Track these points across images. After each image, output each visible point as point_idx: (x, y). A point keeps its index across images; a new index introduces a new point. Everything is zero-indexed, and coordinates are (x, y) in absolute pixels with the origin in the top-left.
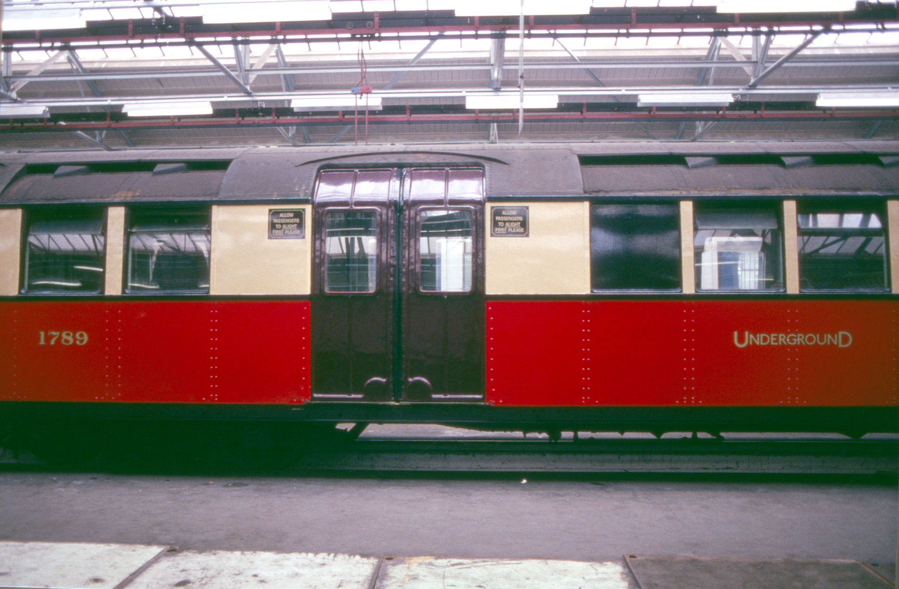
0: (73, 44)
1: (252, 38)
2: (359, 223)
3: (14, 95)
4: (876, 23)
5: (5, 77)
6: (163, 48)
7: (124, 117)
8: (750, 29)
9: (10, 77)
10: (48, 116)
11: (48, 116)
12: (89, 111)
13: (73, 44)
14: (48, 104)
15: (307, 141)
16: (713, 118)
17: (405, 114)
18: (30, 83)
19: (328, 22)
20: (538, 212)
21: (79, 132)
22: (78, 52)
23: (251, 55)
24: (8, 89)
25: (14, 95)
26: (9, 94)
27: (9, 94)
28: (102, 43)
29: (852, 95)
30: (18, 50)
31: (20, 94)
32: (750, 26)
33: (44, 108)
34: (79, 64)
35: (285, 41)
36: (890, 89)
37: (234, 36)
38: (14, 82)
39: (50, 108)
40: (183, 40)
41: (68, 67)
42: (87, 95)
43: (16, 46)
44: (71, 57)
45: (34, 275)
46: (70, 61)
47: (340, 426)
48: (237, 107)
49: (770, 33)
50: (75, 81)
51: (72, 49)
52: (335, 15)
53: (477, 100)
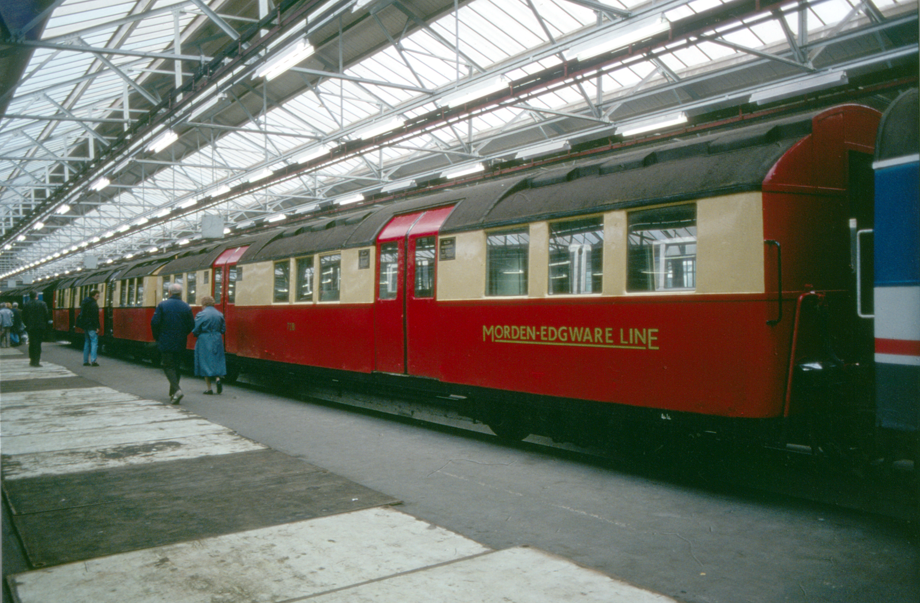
0: (654, 51)
3: (810, 66)
4: (642, 53)
5: (801, 48)
6: (752, 28)
11: (416, 185)
13: (654, 51)
14: (570, 138)
17: (738, 114)
18: (829, 47)
20: (702, 205)
25: (810, 66)
26: (805, 65)
27: (805, 65)
28: (746, 21)
29: (663, 118)
30: (607, 72)
31: (480, 152)
33: (841, 73)
35: (584, 79)
36: (830, 70)
37: (574, 77)
40: (769, 13)
42: (888, 48)
43: (604, 68)
45: (566, 280)
47: (817, 366)
50: (671, 90)
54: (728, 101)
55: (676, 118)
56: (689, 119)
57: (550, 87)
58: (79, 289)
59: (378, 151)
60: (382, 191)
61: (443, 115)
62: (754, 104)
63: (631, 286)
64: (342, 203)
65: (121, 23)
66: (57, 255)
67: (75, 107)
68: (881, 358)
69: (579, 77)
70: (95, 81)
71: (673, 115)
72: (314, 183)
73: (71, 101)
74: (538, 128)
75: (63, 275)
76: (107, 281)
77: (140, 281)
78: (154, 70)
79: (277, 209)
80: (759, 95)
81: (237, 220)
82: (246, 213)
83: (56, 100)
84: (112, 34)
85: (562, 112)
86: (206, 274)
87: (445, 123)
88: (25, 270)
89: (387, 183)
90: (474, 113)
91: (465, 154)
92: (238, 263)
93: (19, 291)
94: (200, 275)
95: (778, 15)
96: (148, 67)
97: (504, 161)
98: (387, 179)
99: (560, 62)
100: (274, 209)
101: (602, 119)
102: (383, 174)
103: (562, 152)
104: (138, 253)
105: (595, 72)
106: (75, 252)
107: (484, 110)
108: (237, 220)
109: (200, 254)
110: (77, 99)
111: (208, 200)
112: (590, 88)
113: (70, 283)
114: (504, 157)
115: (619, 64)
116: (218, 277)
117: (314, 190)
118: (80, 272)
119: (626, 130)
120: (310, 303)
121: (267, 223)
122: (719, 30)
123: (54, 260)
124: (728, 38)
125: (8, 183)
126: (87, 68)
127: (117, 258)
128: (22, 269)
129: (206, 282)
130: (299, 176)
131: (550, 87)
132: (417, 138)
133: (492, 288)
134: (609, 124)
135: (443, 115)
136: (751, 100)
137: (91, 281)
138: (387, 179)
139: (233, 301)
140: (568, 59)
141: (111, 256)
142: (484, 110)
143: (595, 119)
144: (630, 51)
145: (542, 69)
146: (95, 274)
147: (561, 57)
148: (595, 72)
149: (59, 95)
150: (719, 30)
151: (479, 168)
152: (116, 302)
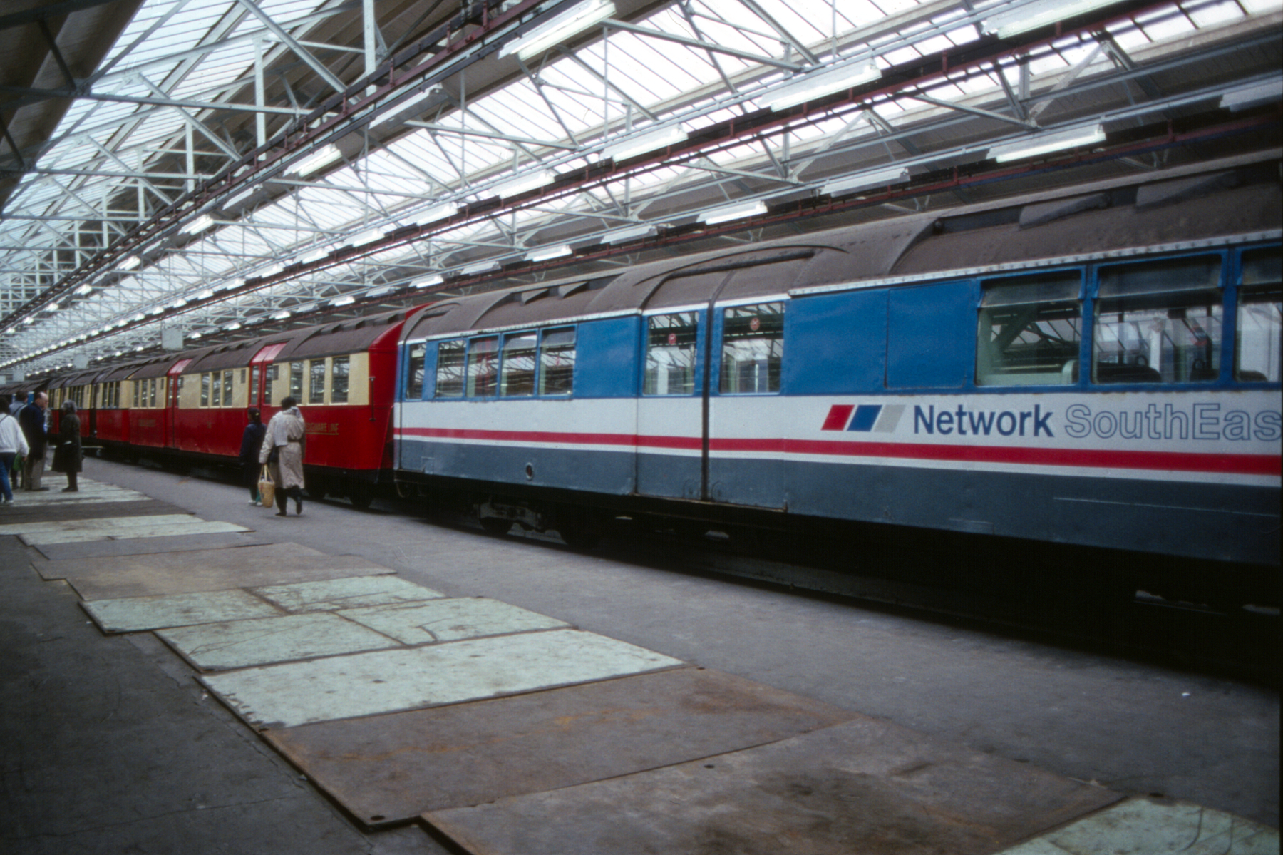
1: (792, 124)
2: (738, 330)
3: (1033, 123)
4: (885, 93)
7: (993, 164)
8: (692, 154)
9: (1027, 100)
10: (908, 179)
11: (908, 179)
12: (1141, 123)
15: (479, 291)
16: (640, 250)
19: (879, 80)
21: (887, 205)
22: (877, 109)
23: (1032, 78)
24: (1025, 116)
25: (635, 218)
26: (1027, 123)
27: (1027, 123)
30: (634, 175)
31: (800, 178)
32: (985, 62)
33: (902, 170)
34: (885, 122)
35: (768, 136)
37: (757, 132)
38: (1032, 106)
39: (909, 168)
41: (871, 130)
42: (1139, 100)
43: (1033, 52)
44: (1115, 52)
46: (1111, 56)
48: (798, 199)
49: (1023, 62)
51: (1109, 37)
52: (690, 134)
53: (713, 216)
54: (965, 155)
55: (753, 208)
56: (1108, 135)
57: (722, 145)
58: (68, 390)
59: (781, 137)
60: (603, 242)
61: (605, 170)
62: (1226, 110)
63: (334, 400)
64: (536, 259)
65: (182, 58)
66: (54, 347)
67: (232, 35)
68: (397, 437)
69: (868, 101)
70: (208, 58)
71: (1086, 129)
72: (428, 248)
73: (117, 139)
74: (716, 186)
75: (54, 371)
76: (92, 383)
77: (118, 384)
78: (167, 149)
79: (379, 282)
80: (1234, 96)
81: (247, 315)
82: (338, 286)
83: (151, 79)
84: (206, 31)
85: (470, 242)
86: (243, 372)
87: (1129, 23)
88: (19, 362)
89: (636, 223)
90: (792, 124)
91: (621, 218)
92: (275, 361)
93: (9, 389)
94: (236, 373)
95: (998, 69)
96: (161, 147)
97: (670, 226)
98: (370, 284)
99: (740, 113)
100: (375, 282)
101: (789, 179)
102: (516, 240)
103: (493, 272)
104: (149, 346)
105: (780, 128)
106: (108, 333)
107: (830, 113)
108: (247, 315)
109: (151, 363)
110: (123, 140)
111: (300, 267)
112: (776, 143)
113: (60, 383)
114: (671, 222)
115: (716, 147)
116: (256, 373)
117: (428, 257)
118: (119, 358)
119: (1002, 153)
120: (925, 402)
121: (702, 225)
122: (922, 85)
123: (50, 352)
124: (932, 94)
125: (103, 153)
126: (201, 34)
127: (126, 351)
128: (14, 361)
129: (243, 381)
130: (410, 242)
131: (722, 145)
132: (744, 147)
133: (136, 404)
134: (796, 186)
135: (605, 170)
136: (1223, 104)
137: (78, 383)
138: (370, 284)
139: (269, 402)
140: (986, 32)
141: (119, 348)
142: (830, 113)
143: (1017, 121)
144: (851, 94)
145: (949, 45)
146: (84, 375)
147: (743, 108)
148: (780, 128)
149: (156, 74)
150: (922, 85)
151: (438, 280)
152: (99, 406)
